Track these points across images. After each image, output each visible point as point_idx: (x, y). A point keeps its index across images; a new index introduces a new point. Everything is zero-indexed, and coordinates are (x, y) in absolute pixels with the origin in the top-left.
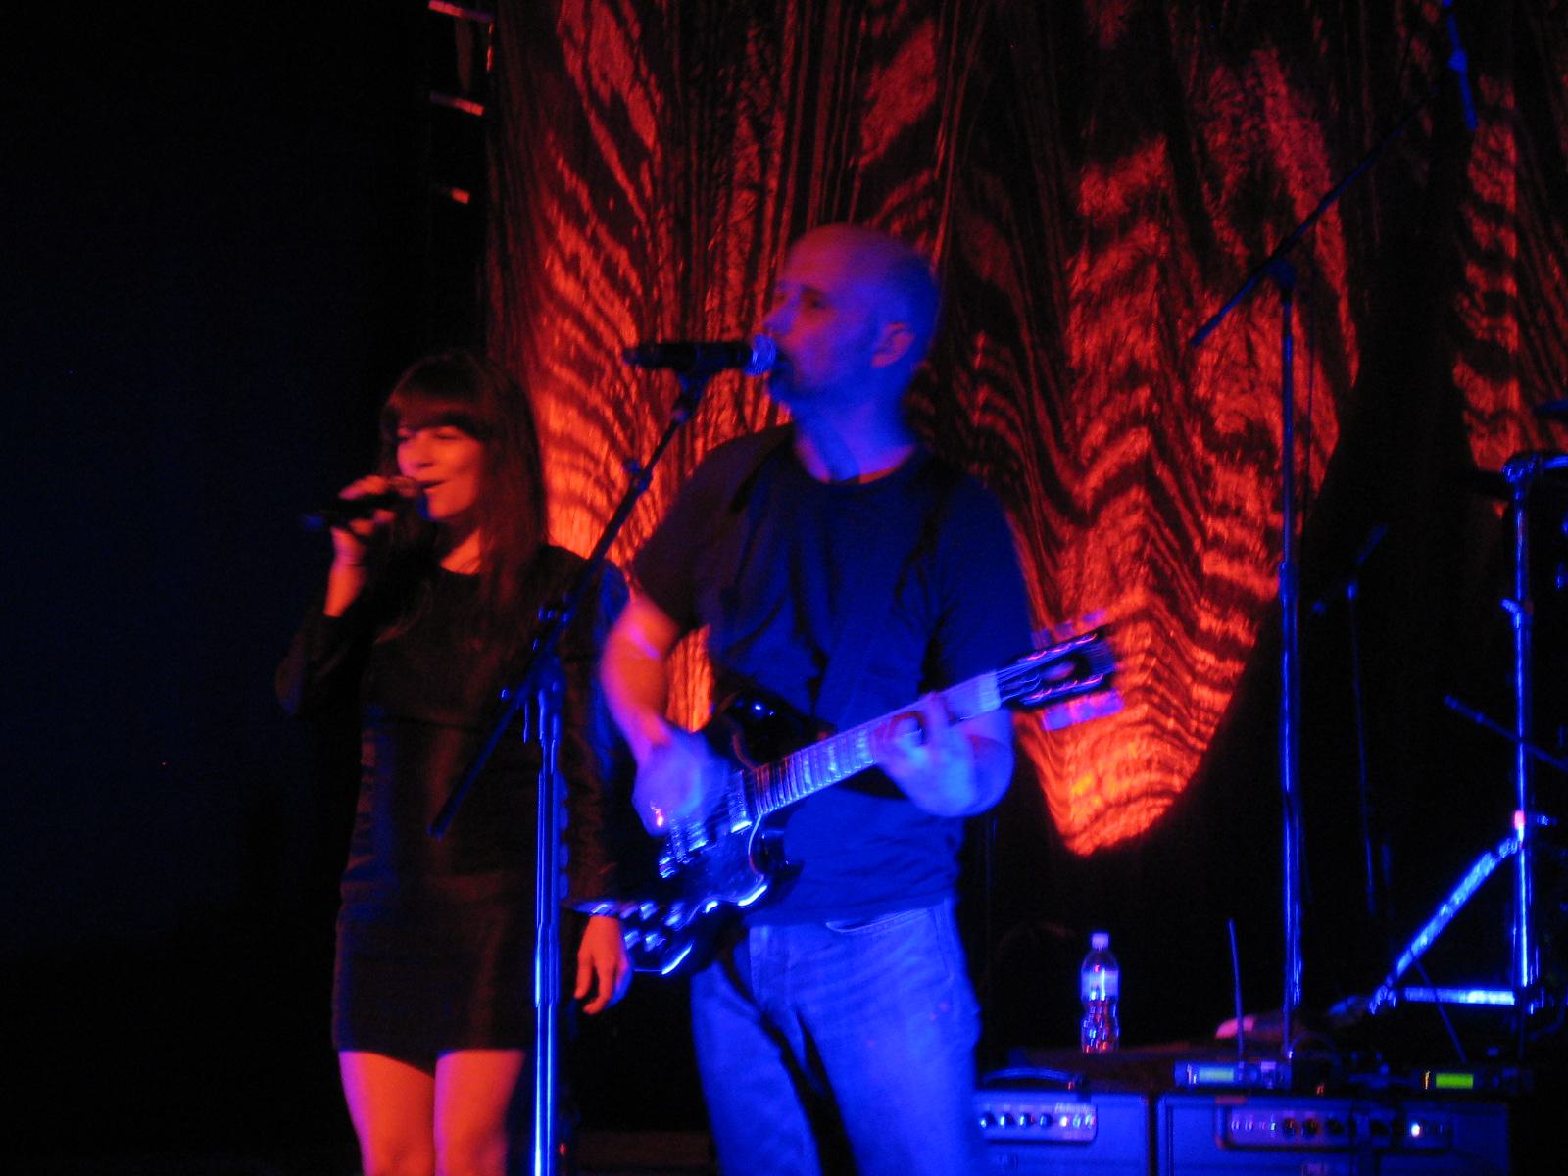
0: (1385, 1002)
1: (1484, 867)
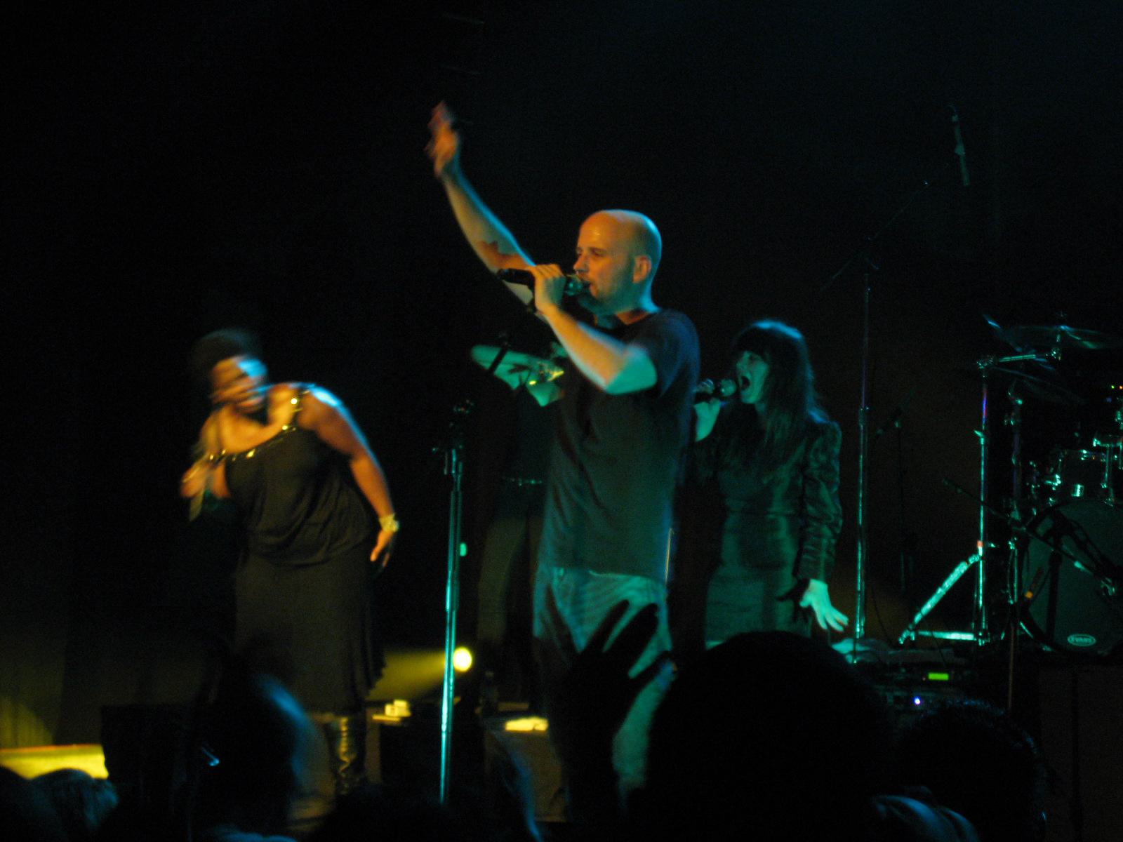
0: (909, 638)
1: (962, 569)
